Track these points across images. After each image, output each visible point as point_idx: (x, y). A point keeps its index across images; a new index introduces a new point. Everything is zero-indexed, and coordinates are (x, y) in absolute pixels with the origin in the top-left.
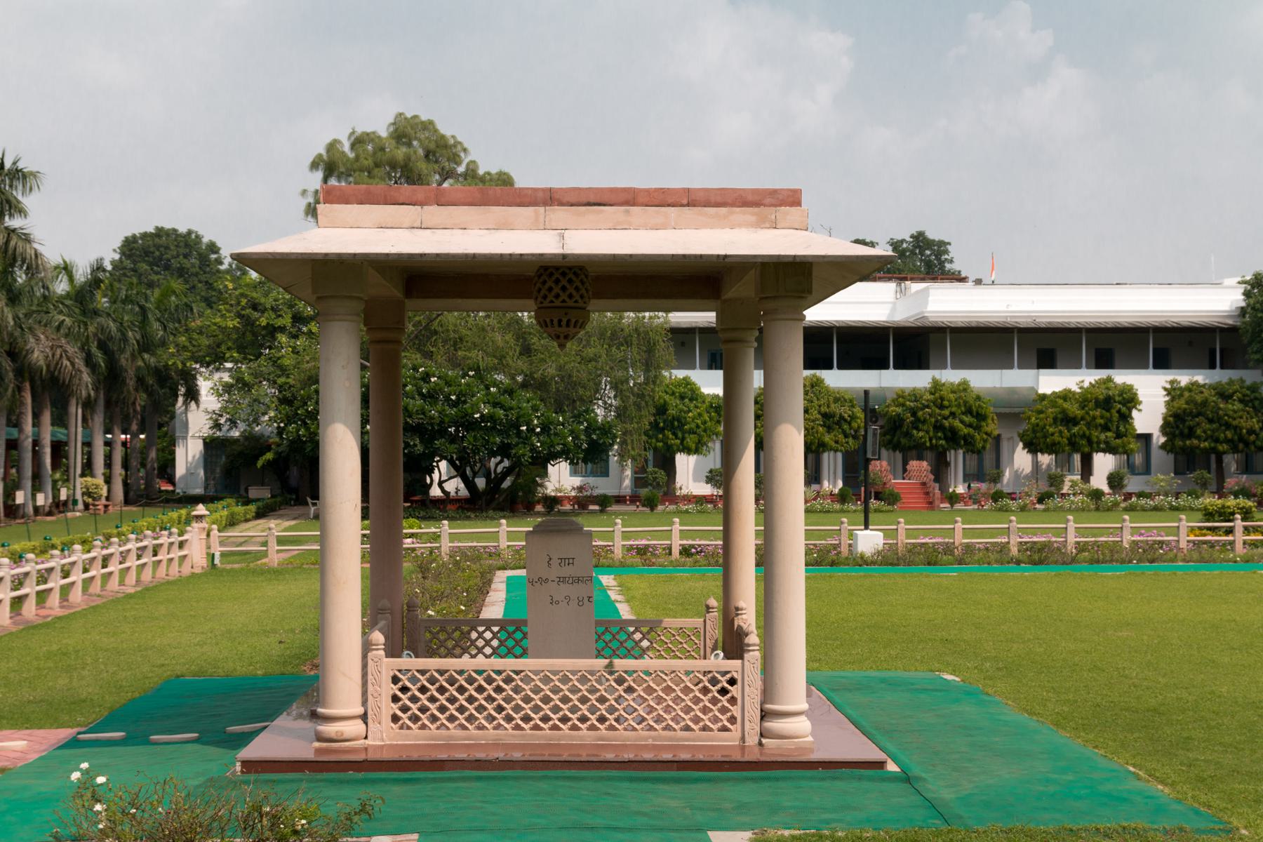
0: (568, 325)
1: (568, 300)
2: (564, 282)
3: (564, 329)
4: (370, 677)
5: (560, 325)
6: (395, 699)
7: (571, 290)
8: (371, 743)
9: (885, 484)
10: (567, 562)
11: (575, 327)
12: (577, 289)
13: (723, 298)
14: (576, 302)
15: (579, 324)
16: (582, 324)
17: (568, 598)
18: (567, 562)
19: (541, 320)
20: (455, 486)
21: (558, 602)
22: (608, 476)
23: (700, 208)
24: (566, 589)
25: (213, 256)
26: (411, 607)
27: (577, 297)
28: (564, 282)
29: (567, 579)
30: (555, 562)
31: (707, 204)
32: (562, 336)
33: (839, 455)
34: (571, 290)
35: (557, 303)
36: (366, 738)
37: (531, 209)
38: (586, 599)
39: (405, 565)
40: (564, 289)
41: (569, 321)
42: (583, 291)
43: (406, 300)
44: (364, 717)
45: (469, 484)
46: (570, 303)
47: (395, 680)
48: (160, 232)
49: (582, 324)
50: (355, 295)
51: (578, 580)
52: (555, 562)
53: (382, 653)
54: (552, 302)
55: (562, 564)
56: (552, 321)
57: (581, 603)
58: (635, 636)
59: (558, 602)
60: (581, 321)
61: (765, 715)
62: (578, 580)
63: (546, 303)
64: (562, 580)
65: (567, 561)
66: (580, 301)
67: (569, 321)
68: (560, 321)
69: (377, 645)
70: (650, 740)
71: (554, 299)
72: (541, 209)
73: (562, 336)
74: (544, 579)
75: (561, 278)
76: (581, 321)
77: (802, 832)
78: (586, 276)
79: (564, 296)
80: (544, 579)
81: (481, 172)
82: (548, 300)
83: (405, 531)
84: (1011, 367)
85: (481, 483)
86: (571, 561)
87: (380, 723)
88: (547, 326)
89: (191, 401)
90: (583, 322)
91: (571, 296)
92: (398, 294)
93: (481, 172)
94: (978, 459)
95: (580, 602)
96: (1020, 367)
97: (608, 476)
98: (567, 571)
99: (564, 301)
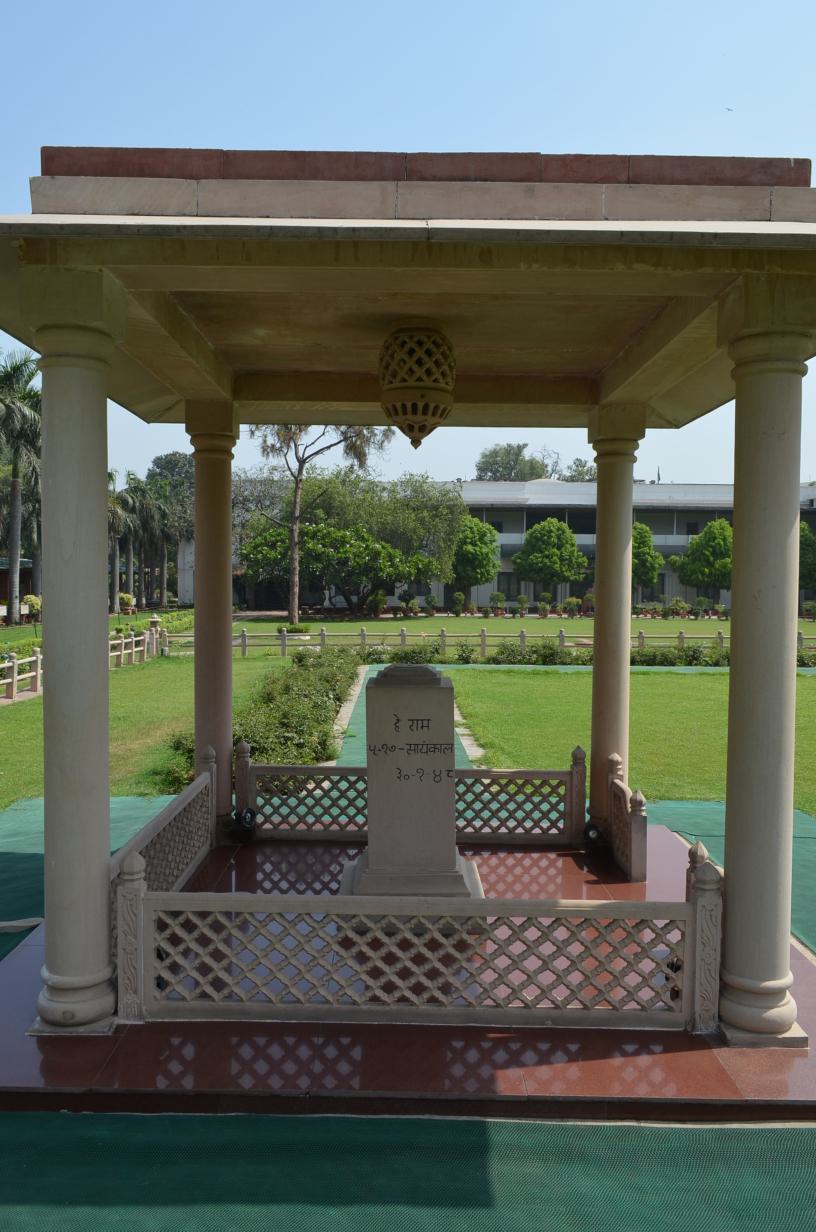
0: (425, 412)
1: (424, 377)
2: (420, 353)
3: (419, 418)
4: (120, 923)
5: (405, 413)
6: (161, 955)
7: (429, 364)
8: (123, 1022)
10: (420, 725)
11: (434, 414)
12: (437, 363)
13: (605, 401)
14: (436, 381)
15: (440, 412)
16: (443, 412)
18: (420, 725)
19: (390, 406)
20: (340, 601)
21: (407, 777)
22: (416, 448)
23: (648, 186)
26: (239, 753)
27: (437, 375)
28: (420, 353)
29: (420, 747)
31: (660, 180)
32: (416, 427)
33: (568, 585)
34: (429, 364)
35: (411, 382)
36: (115, 1013)
37: (376, 184)
38: (444, 774)
39: (115, 802)
40: (419, 362)
41: (426, 407)
42: (445, 367)
43: (236, 404)
44: (113, 984)
45: (348, 601)
46: (428, 382)
47: (162, 926)
48: (175, 454)
49: (443, 412)
50: (94, 324)
51: (435, 748)
52: (404, 725)
53: (143, 885)
54: (404, 380)
55: (414, 727)
56: (404, 406)
57: (438, 779)
58: (569, 949)
59: (407, 777)
60: (442, 407)
61: (725, 988)
62: (435, 748)
63: (397, 383)
64: (413, 748)
66: (441, 380)
67: (426, 407)
68: (415, 406)
69: (132, 874)
70: (549, 1022)
71: (406, 377)
72: (390, 185)
73: (416, 427)
74: (390, 746)
75: (417, 349)
76: (442, 407)
78: (451, 368)
79: (420, 372)
80: (390, 746)
82: (399, 378)
84: (672, 533)
85: (354, 599)
87: (135, 992)
88: (397, 414)
90: (445, 409)
91: (429, 372)
92: (225, 394)
96: (678, 533)
97: (416, 448)
98: (419, 736)
99: (420, 379)
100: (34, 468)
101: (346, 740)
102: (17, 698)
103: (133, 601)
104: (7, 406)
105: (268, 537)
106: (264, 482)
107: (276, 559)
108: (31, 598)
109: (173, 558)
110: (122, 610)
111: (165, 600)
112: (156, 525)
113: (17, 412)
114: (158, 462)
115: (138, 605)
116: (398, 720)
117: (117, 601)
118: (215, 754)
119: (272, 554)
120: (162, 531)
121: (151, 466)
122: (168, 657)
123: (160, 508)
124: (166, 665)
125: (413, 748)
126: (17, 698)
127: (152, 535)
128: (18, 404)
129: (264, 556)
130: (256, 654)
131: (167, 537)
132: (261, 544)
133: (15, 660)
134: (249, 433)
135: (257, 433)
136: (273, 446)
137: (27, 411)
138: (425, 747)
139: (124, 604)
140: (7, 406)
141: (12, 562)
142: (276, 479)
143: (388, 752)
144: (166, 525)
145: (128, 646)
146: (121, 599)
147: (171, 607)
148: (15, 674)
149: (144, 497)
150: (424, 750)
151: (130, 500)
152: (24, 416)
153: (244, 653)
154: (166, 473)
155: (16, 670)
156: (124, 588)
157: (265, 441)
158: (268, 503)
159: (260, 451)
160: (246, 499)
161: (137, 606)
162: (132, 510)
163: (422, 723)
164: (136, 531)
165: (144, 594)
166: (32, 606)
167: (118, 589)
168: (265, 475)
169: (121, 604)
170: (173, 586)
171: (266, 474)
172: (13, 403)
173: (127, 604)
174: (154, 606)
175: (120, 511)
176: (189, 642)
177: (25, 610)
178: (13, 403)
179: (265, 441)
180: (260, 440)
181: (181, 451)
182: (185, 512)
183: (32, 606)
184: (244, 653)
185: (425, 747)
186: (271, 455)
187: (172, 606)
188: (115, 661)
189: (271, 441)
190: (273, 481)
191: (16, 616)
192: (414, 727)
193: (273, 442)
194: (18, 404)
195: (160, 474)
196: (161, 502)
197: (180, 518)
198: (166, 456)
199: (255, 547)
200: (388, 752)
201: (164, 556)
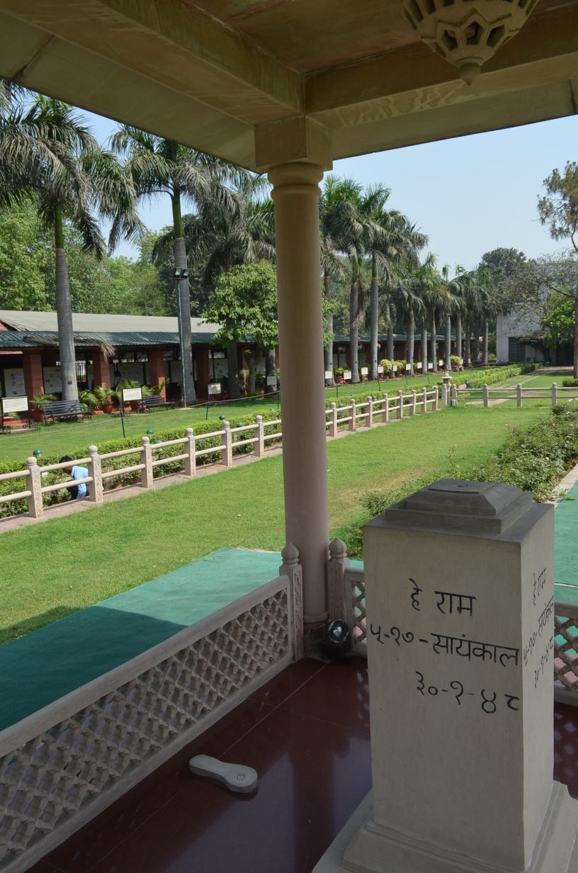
9: (274, 263)
17: (459, 689)
21: (434, 691)
24: (448, 667)
25: (522, 257)
29: (456, 643)
30: (428, 599)
38: (502, 702)
48: (499, 250)
51: (480, 650)
52: (428, 599)
55: (446, 606)
59: (434, 691)
62: (480, 650)
64: (444, 643)
65: (456, 600)
74: (404, 632)
77: (320, 124)
80: (404, 632)
81: (387, 208)
83: (280, 421)
86: (466, 603)
89: (7, 414)
93: (387, 208)
94: (25, 372)
95: (488, 703)
98: (455, 625)
100: (385, 268)
101: (563, 503)
102: (374, 426)
103: (461, 362)
104: (364, 226)
105: (565, 307)
106: (564, 264)
107: (572, 324)
108: (386, 361)
109: (493, 329)
110: (452, 368)
111: (486, 360)
112: (478, 304)
113: (371, 229)
114: (486, 257)
115: (465, 365)
116: (418, 590)
117: (449, 362)
118: (297, 553)
119: (569, 321)
120: (483, 308)
121: (481, 260)
122: (455, 407)
123: (481, 291)
124: (452, 415)
125: (444, 643)
126: (374, 426)
127: (475, 312)
128: (372, 224)
129: (562, 323)
130: (530, 406)
131: (487, 313)
132: (560, 313)
133: (354, 404)
134: (540, 221)
135: (547, 220)
136: (561, 229)
137: (378, 228)
138: (465, 645)
139: (454, 364)
140: (364, 226)
141: (409, 338)
142: (575, 260)
143: (401, 640)
144: (485, 304)
145: (420, 399)
146: (452, 360)
147: (491, 365)
148: (336, 418)
149: (468, 283)
150: (464, 650)
151: (458, 287)
152: (376, 232)
153: (519, 404)
154: (492, 264)
155: (336, 415)
156: (454, 352)
157: (554, 226)
158: (568, 280)
159: (550, 234)
160: (550, 279)
161: (464, 365)
162: (459, 294)
163: (462, 603)
164: (462, 311)
165: (470, 356)
166: (385, 367)
167: (450, 353)
168: (566, 258)
169: (452, 364)
170: (493, 349)
171: (567, 256)
172: (369, 223)
173: (457, 364)
174: (478, 365)
175: (449, 295)
176: (275, 426)
177: (381, 370)
178: (369, 223)
179: (554, 226)
180: (549, 226)
181: (504, 247)
182: (502, 292)
183: (385, 367)
184: (519, 404)
185: (465, 645)
186: (559, 236)
187: (493, 364)
188: (420, 409)
189: (558, 225)
190: (573, 262)
191: (376, 375)
192: (446, 606)
193: (561, 226)
194: (372, 224)
195: (488, 266)
196: (484, 288)
197: (497, 297)
198: (493, 252)
199: (554, 316)
200: (401, 640)
201: (485, 327)
